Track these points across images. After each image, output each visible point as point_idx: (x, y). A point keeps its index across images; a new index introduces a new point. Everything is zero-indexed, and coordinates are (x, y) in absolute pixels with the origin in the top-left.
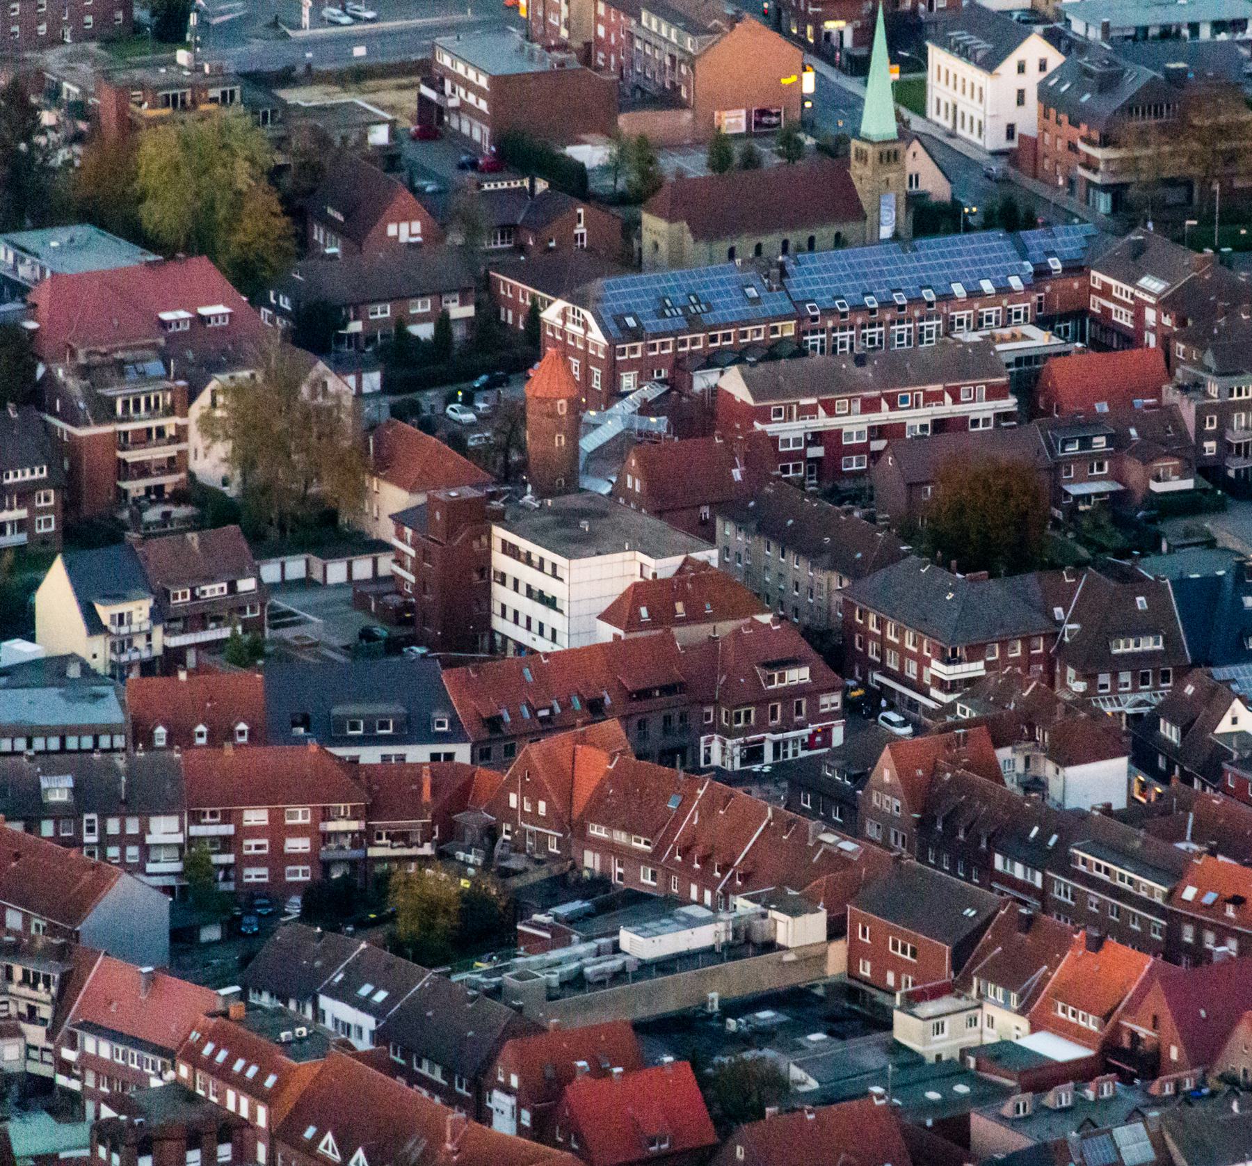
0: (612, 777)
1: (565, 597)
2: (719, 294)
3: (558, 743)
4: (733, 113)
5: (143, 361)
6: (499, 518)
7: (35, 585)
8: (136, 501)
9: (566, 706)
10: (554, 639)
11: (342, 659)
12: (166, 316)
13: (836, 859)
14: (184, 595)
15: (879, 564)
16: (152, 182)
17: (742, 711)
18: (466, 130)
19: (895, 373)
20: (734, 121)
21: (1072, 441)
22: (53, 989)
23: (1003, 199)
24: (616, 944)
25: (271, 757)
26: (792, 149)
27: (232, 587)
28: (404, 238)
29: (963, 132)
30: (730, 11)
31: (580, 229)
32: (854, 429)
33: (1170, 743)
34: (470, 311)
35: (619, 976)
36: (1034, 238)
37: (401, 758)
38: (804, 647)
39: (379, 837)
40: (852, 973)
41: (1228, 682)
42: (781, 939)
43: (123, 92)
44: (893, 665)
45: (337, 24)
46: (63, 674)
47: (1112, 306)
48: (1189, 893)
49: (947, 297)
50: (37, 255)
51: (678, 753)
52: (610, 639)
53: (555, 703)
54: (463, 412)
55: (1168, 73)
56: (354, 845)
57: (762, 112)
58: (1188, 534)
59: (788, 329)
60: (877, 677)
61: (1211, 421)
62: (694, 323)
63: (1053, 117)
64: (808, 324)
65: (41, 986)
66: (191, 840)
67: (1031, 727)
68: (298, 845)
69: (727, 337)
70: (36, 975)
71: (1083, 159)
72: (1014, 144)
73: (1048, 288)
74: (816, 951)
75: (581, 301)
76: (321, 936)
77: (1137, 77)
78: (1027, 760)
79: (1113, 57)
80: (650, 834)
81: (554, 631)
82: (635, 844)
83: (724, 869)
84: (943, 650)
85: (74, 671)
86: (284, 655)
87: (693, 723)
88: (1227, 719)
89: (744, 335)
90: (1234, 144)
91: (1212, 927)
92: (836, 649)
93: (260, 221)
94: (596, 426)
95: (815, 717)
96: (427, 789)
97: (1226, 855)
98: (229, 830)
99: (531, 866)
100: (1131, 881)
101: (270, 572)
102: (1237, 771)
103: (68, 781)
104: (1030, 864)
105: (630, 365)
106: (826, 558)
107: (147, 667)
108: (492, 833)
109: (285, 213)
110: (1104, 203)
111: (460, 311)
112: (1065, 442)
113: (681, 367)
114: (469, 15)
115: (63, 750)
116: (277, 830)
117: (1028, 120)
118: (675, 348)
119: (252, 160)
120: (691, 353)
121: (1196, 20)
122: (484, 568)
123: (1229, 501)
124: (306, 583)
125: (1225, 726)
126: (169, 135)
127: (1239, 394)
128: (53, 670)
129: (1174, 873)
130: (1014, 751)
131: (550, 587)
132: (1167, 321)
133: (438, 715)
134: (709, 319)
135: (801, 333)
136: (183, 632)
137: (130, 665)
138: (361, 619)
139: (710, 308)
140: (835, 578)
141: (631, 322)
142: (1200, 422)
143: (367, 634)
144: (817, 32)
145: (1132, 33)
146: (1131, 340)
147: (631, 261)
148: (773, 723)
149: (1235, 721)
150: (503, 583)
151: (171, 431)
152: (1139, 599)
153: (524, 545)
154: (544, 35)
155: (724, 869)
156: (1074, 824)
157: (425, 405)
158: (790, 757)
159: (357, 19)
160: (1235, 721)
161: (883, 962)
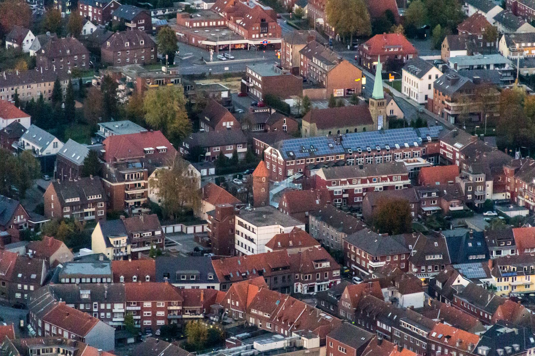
0: (258, 295)
1: (256, 238)
3: (244, 284)
4: (339, 90)
6: (238, 213)
7: (91, 232)
9: (251, 272)
10: (253, 252)
11: (185, 256)
12: (146, 149)
13: (324, 321)
14: (138, 235)
15: (358, 230)
16: (148, 108)
18: (255, 94)
19: (372, 171)
20: (339, 93)
21: (425, 194)
23: (417, 120)
24: (253, 346)
25: (157, 285)
26: (355, 100)
27: (153, 233)
28: (228, 127)
30: (339, 58)
31: (285, 125)
32: (358, 189)
34: (245, 150)
36: (423, 130)
38: (327, 255)
39: (187, 312)
41: (457, 270)
42: (305, 346)
43: (144, 79)
45: (222, 60)
46: (98, 259)
47: (446, 152)
48: (434, 334)
49: (394, 148)
52: (266, 252)
53: (247, 271)
54: (238, 181)
56: (179, 314)
57: (349, 90)
58: (460, 223)
59: (342, 157)
60: (353, 266)
61: (470, 188)
62: (312, 154)
64: (349, 156)
66: (127, 311)
67: (394, 282)
68: (161, 313)
69: (322, 159)
71: (446, 107)
72: (427, 102)
73: (427, 146)
74: (317, 349)
75: (276, 147)
76: (158, 341)
77: (464, 80)
78: (392, 292)
79: (457, 75)
81: (253, 249)
83: (291, 324)
86: (168, 254)
88: (456, 281)
90: (493, 103)
91: (441, 345)
92: (340, 257)
93: (181, 120)
94: (278, 186)
95: (331, 277)
98: (139, 308)
99: (233, 322)
100: (417, 330)
101: (170, 229)
102: (458, 297)
103: (89, 292)
104: (388, 325)
105: (291, 167)
106: (341, 229)
107: (126, 258)
108: (222, 311)
109: (189, 118)
110: (452, 120)
111: (241, 150)
113: (307, 169)
114: (263, 58)
115: (70, 282)
116: (154, 309)
117: (431, 94)
120: (311, 164)
121: (488, 63)
122: (233, 229)
124: (181, 233)
125: (455, 283)
126: (154, 92)
127: (479, 179)
128: (95, 259)
129: (429, 328)
131: (252, 236)
132: (462, 157)
134: (317, 153)
136: (138, 247)
137: (120, 257)
138: (196, 244)
140: (343, 234)
141: (291, 154)
142: (467, 188)
143: (196, 249)
144: (371, 65)
145: (468, 67)
146: (452, 162)
147: (298, 134)
148: (317, 279)
149: (459, 281)
150: (238, 234)
151: (142, 185)
152: (436, 243)
153: (245, 222)
154: (285, 65)
155: (291, 324)
156: (403, 312)
157: (227, 179)
158: (323, 290)
159: (228, 58)
160: (459, 281)
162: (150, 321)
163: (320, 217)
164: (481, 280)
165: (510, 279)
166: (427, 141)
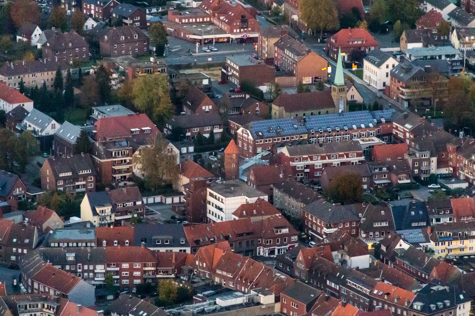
0: (223, 257)
1: (225, 207)
2: (286, 127)
3: (211, 247)
4: (308, 78)
5: (122, 141)
6: (209, 186)
8: (118, 180)
10: (222, 220)
12: (132, 130)
13: (280, 280)
14: (121, 205)
17: (269, 240)
19: (331, 149)
20: (307, 80)
22: (55, 310)
25: (134, 249)
27: (135, 203)
28: (207, 110)
29: (372, 84)
31: (257, 109)
32: (318, 164)
33: (383, 251)
34: (221, 130)
35: (214, 311)
36: (378, 113)
37: (171, 251)
38: (287, 223)
39: (160, 272)
40: (282, 312)
41: (400, 235)
42: (262, 302)
44: (314, 229)
45: (206, 52)
47: (398, 132)
48: (375, 292)
50: (104, 113)
51: (250, 251)
53: (215, 237)
55: (426, 69)
57: (316, 78)
59: (305, 137)
60: (310, 232)
61: (417, 164)
62: (278, 134)
63: (394, 80)
64: (311, 135)
65: (52, 309)
66: (107, 272)
68: (137, 274)
69: (288, 138)
70: (51, 307)
71: (401, 92)
72: (384, 88)
75: (247, 128)
76: (131, 298)
77: (416, 69)
78: (342, 255)
79: (411, 64)
80: (232, 273)
81: (222, 217)
82: (228, 275)
83: (250, 283)
84: (327, 225)
85: (88, 226)
87: (255, 243)
89: (293, 138)
92: (299, 225)
93: (165, 104)
95: (290, 242)
96: (174, 259)
97: (388, 281)
98: (118, 269)
100: (361, 288)
102: (399, 259)
103: (74, 255)
104: (336, 283)
105: (260, 146)
108: (191, 271)
110: (406, 104)
111: (217, 130)
112: (375, 169)
114: (243, 50)
117: (388, 81)
118: (273, 141)
119: (163, 88)
120: (277, 143)
123: (421, 186)
124: (161, 203)
125: (398, 247)
128: (83, 226)
129: (372, 286)
130: (338, 252)
131: (221, 205)
133: (182, 239)
134: (283, 133)
135: (309, 138)
136: (121, 215)
139: (283, 130)
141: (260, 134)
142: (413, 164)
143: (173, 217)
145: (422, 58)
146: (402, 141)
149: (401, 245)
150: (210, 204)
151: (128, 161)
152: (382, 212)
153: (215, 194)
154: (262, 56)
155: (250, 283)
157: (203, 156)
160: (401, 245)
161: (289, 309)
162: (128, 281)
163: (282, 190)
164: (420, 244)
165: (447, 243)
166: (381, 122)
